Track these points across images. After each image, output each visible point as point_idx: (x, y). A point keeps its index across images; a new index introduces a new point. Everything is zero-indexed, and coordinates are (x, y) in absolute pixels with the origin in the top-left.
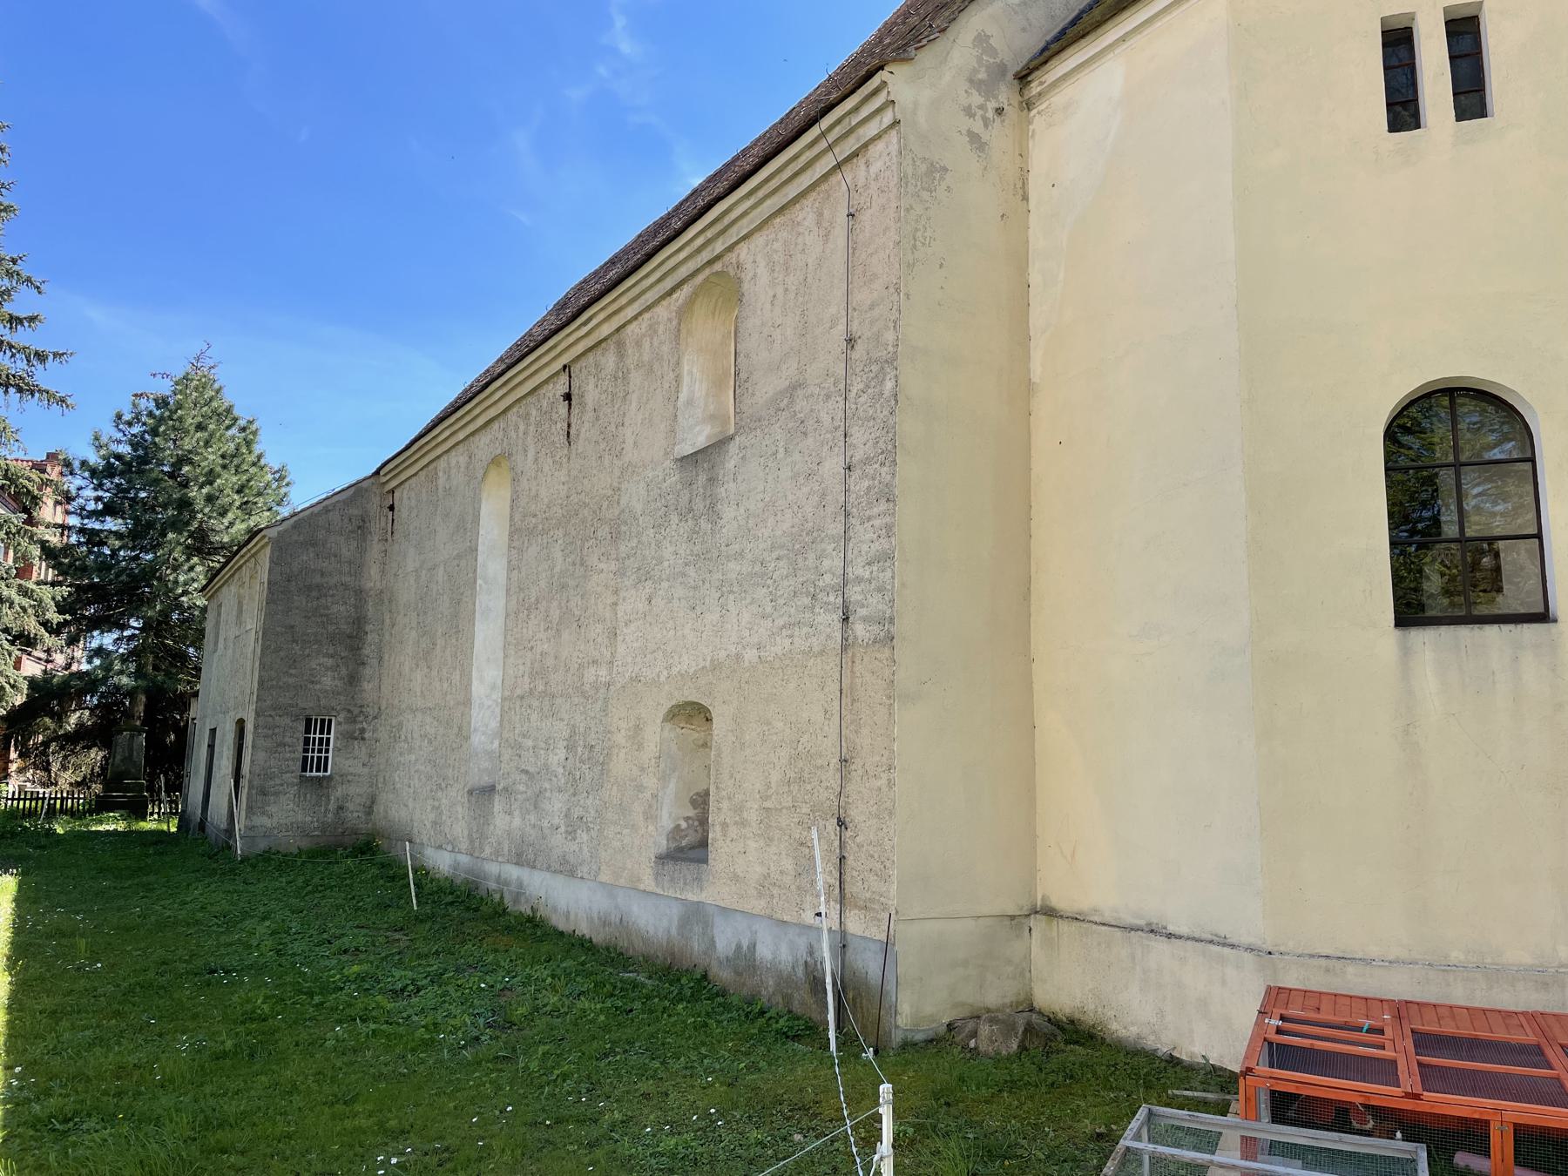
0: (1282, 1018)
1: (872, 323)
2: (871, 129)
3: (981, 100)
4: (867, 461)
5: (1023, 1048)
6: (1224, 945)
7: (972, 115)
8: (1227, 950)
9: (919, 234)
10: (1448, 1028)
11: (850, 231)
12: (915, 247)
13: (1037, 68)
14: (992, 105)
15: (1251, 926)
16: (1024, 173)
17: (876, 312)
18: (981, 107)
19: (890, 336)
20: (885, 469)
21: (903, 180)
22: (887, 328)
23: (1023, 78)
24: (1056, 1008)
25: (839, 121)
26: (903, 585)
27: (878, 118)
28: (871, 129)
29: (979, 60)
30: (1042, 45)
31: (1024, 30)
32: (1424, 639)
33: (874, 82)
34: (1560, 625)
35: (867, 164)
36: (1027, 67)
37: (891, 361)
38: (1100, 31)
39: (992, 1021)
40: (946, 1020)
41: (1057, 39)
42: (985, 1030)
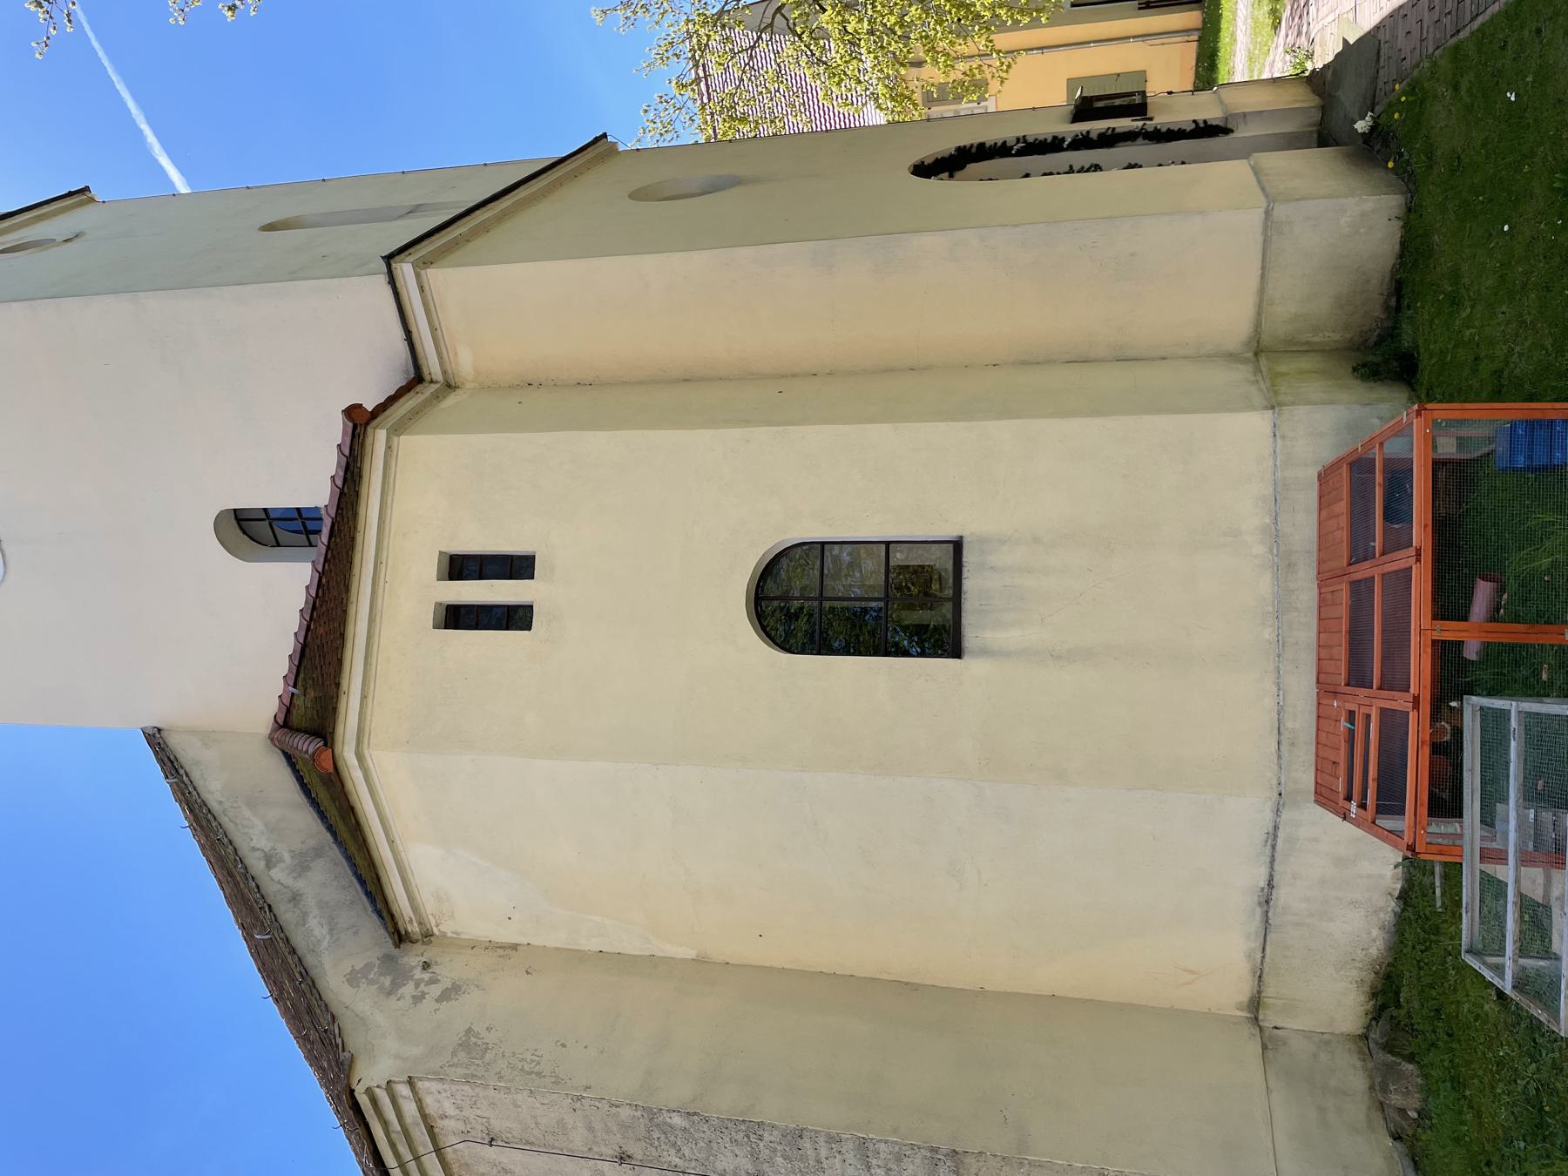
0: (1349, 798)
1: (608, 1132)
2: (410, 1108)
3: (411, 985)
4: (755, 1156)
5: (1411, 1058)
6: (1275, 836)
7: (423, 995)
8: (1281, 834)
9: (527, 1068)
10: (1342, 653)
11: (507, 1145)
12: (538, 1074)
13: (395, 925)
14: (418, 974)
15: (1252, 811)
16: (492, 946)
17: (598, 1126)
18: (417, 986)
19: (625, 1113)
20: (766, 1135)
21: (469, 1080)
22: (616, 1115)
23: (400, 938)
24: (1361, 1010)
25: (393, 1146)
26: (895, 1131)
27: (401, 1102)
28: (410, 1108)
29: (372, 982)
30: (375, 917)
31: (356, 933)
32: (972, 634)
33: (363, 1100)
34: (965, 534)
35: (444, 1117)
36: (391, 935)
37: (651, 1114)
38: (378, 863)
39: (1385, 1090)
40: (1390, 1142)
41: (373, 901)
42: (1396, 1099)
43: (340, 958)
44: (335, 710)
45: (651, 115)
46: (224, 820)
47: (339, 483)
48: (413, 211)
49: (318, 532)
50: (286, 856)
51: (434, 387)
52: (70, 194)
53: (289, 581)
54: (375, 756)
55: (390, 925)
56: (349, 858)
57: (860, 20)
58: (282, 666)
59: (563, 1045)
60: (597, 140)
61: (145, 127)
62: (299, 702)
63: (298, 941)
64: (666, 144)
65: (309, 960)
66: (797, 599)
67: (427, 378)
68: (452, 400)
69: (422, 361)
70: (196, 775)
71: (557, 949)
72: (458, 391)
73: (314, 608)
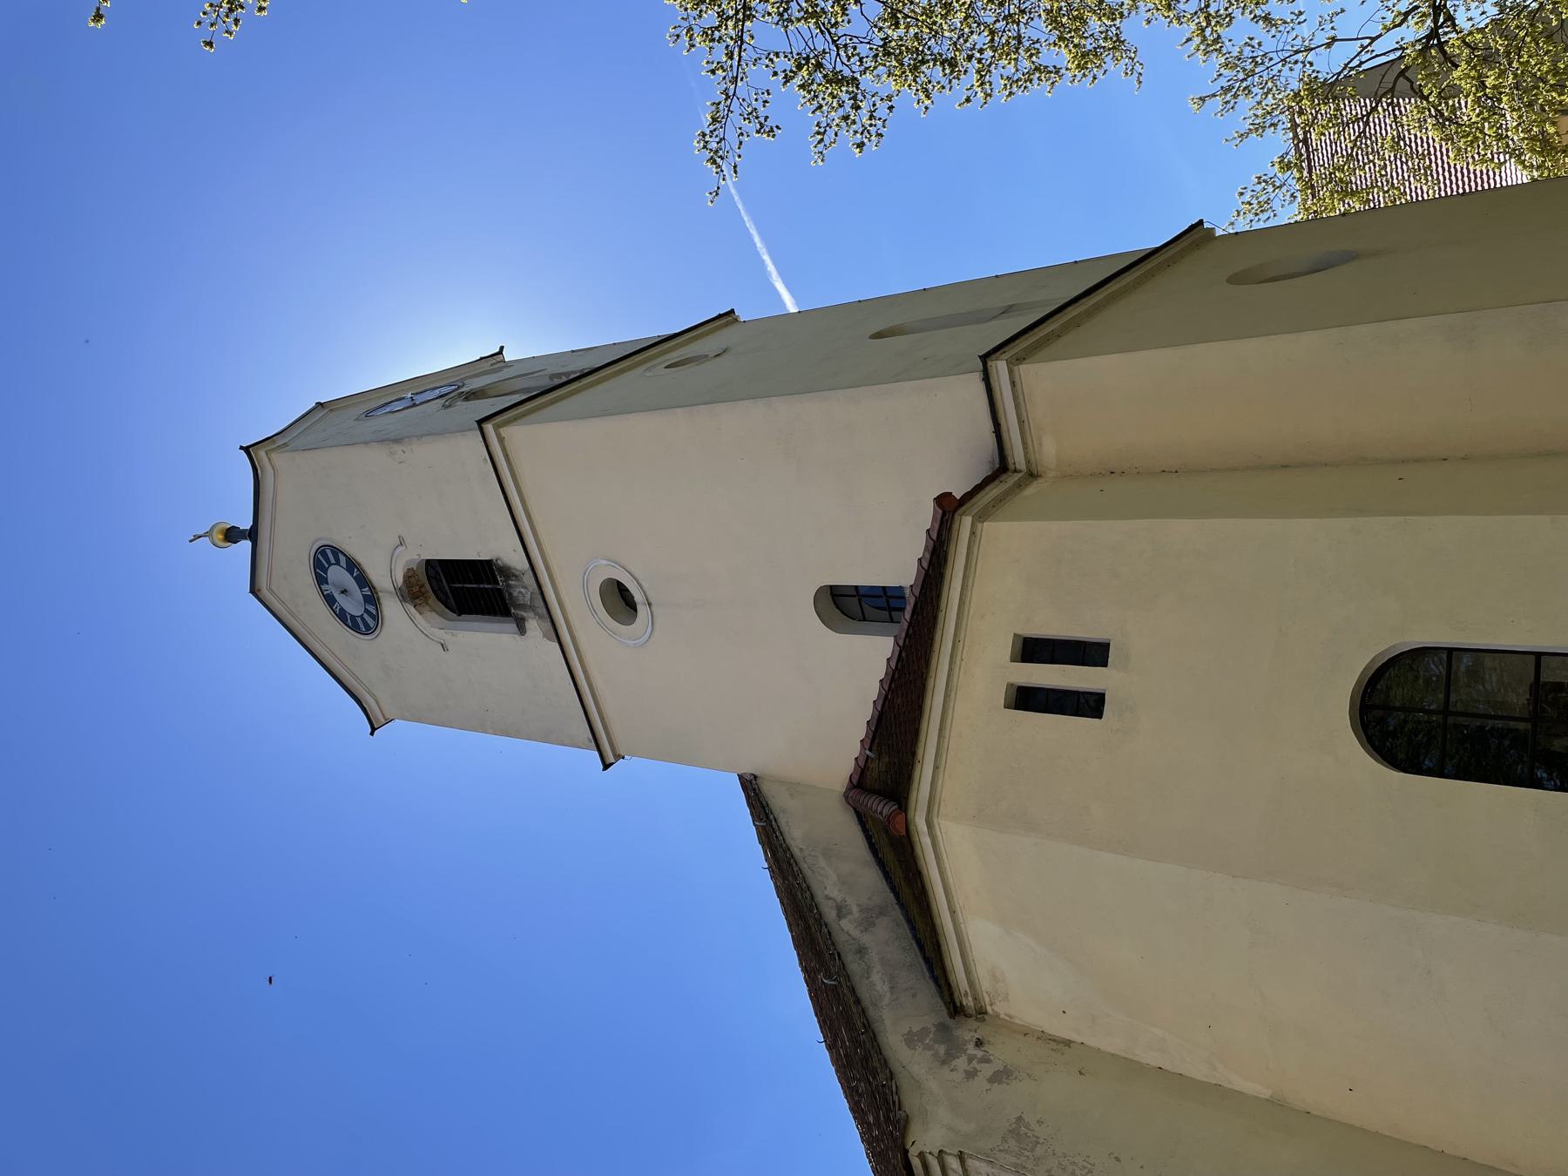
13: (951, 995)
16: (1043, 1037)
18: (970, 1060)
23: (956, 1010)
29: (928, 1047)
30: (932, 983)
31: (914, 996)
33: (916, 1163)
41: (931, 969)
43: (901, 1019)
44: (910, 777)
45: (1247, 198)
46: (804, 866)
47: (925, 565)
48: (1007, 310)
49: (902, 609)
50: (855, 909)
51: (1017, 476)
52: (720, 316)
53: (871, 654)
54: (944, 825)
55: (947, 998)
56: (909, 921)
57: (1502, 74)
58: (861, 732)
59: (1118, 1159)
60: (1192, 227)
61: (766, 258)
62: (873, 765)
63: (863, 993)
64: (1261, 225)
65: (871, 1012)
66: (1398, 709)
67: (1011, 467)
68: (1031, 490)
69: (1008, 452)
70: (782, 820)
71: (1113, 1055)
72: (1040, 480)
73: (893, 680)
